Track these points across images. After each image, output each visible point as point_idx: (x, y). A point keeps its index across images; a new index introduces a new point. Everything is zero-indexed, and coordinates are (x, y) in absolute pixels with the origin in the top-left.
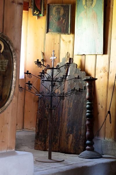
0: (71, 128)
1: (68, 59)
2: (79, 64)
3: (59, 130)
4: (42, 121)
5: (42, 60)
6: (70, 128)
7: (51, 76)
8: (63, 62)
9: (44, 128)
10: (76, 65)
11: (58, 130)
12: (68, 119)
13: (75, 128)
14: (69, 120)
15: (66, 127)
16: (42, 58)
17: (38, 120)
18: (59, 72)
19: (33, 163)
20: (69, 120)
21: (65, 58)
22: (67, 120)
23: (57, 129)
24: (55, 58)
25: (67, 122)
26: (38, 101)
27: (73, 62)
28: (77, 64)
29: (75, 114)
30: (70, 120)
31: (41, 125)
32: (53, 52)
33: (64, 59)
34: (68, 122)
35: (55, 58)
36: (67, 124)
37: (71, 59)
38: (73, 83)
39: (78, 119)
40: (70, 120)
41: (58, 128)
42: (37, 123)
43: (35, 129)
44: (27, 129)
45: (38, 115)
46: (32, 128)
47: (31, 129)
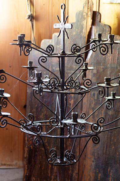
0: (102, 172)
1: (90, 14)
2: (114, 24)
3: (74, 174)
4: (37, 153)
5: (29, 16)
6: (99, 172)
7: (59, 76)
8: (78, 21)
9: (41, 167)
10: (108, 29)
11: (72, 175)
12: (94, 152)
13: (111, 174)
14: (96, 154)
15: (90, 170)
16: (29, 13)
17: (26, 149)
18: (79, 66)
19: (23, 107)
20: (96, 154)
21: (83, 11)
22: (93, 154)
23: (70, 172)
24: (68, 26)
25: (93, 159)
26: (25, 106)
27: (100, 22)
28: (110, 27)
29: (111, 141)
30: (98, 154)
31: (35, 162)
32: (62, 11)
33: (80, 16)
34: (95, 159)
35: (68, 26)
36: (93, 164)
37: (97, 14)
38: (102, 70)
39: (118, 154)
40: (98, 154)
41: (73, 171)
42: (25, 156)
43: (21, 163)
44: (5, 165)
45: (26, 139)
46: (14, 163)
47: (12, 165)
